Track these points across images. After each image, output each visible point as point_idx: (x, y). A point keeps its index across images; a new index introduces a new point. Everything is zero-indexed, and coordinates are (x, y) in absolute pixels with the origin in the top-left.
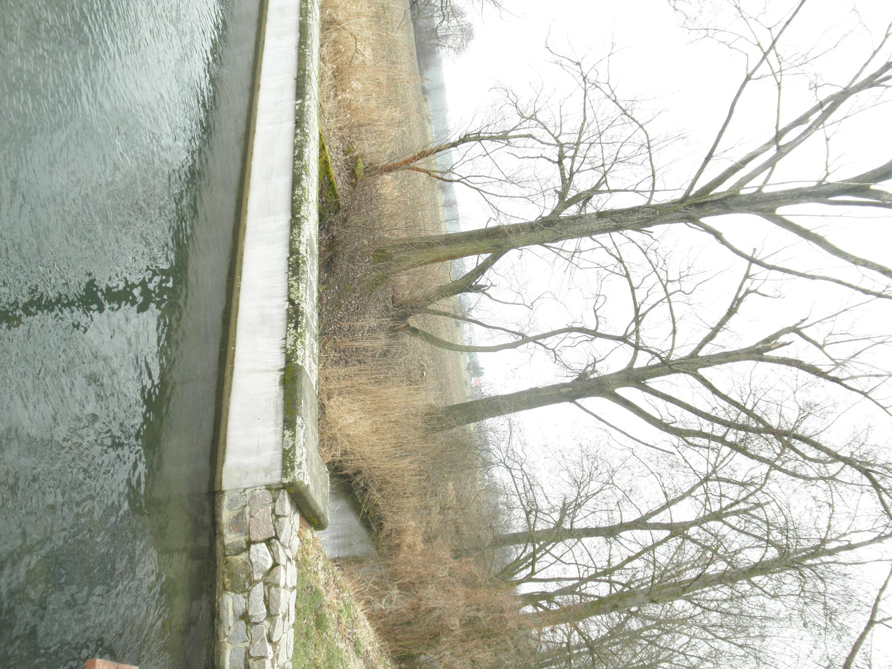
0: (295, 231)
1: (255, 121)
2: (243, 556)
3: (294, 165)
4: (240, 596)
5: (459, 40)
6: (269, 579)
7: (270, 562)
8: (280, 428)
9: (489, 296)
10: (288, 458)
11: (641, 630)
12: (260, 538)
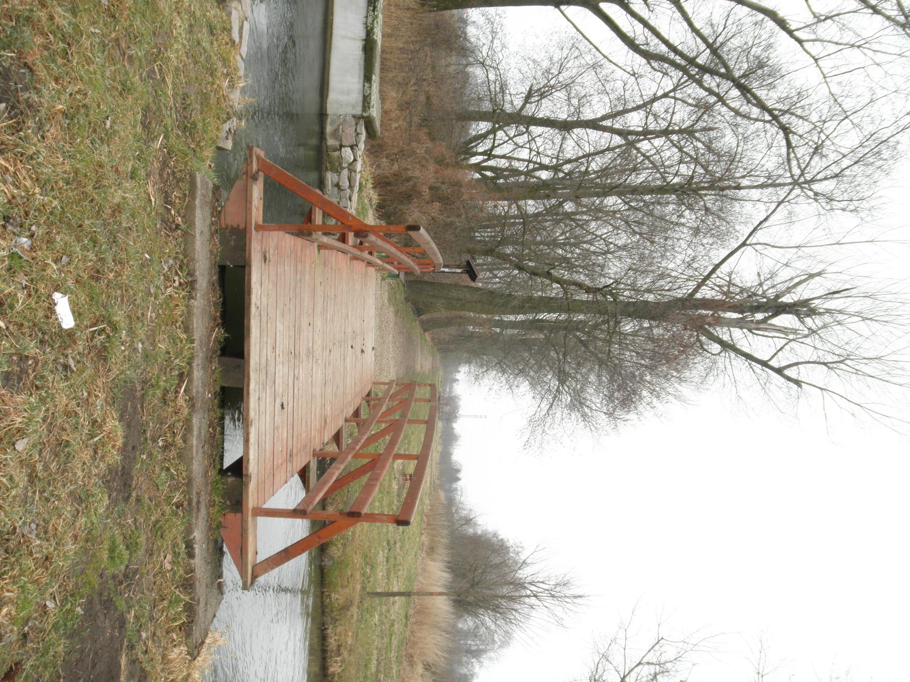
2: (337, 153)
4: (335, 174)
6: (351, 167)
7: (352, 158)
8: (362, 80)
10: (366, 100)
11: (573, 213)
12: (347, 144)
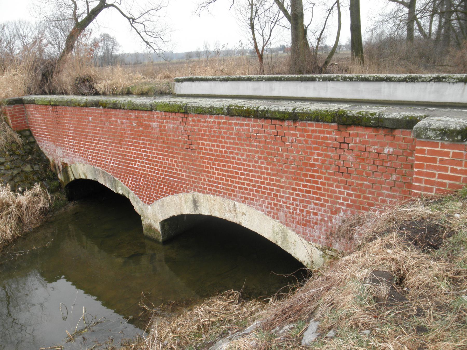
0: (393, 79)
3: (355, 81)
5: (109, 43)
9: (308, 25)
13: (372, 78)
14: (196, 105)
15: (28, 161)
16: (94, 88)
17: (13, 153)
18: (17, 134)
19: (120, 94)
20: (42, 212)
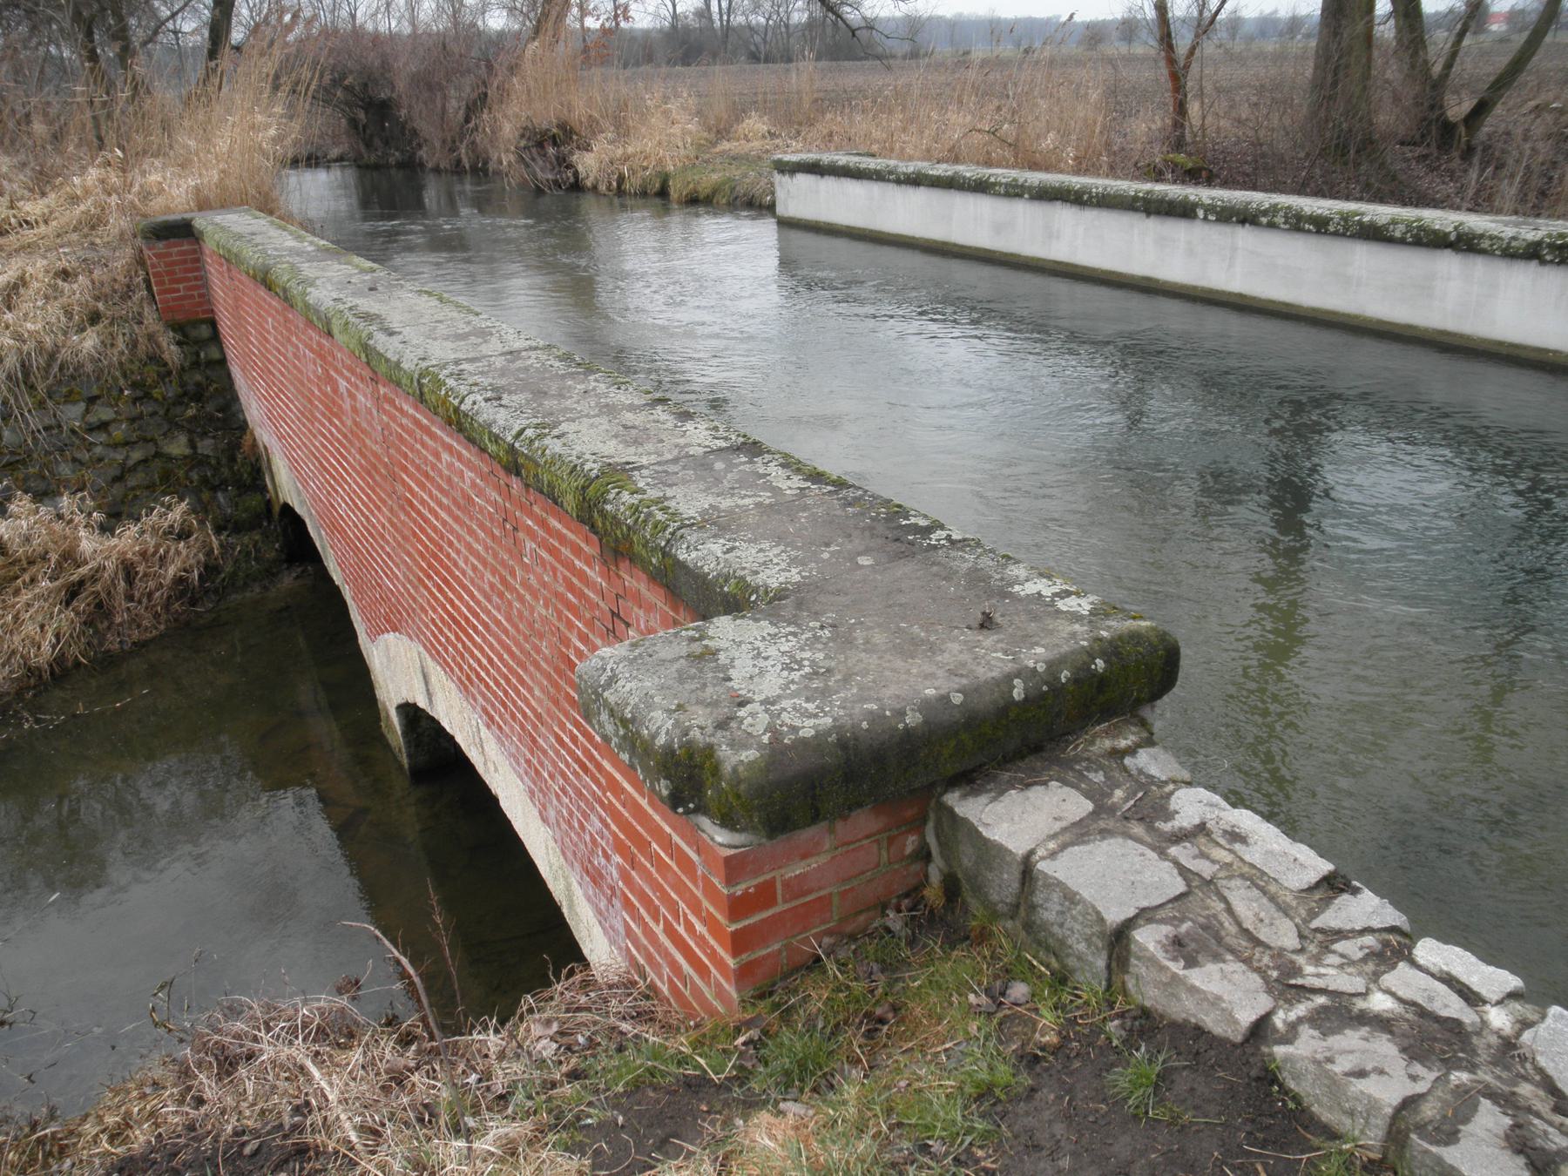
0: (1485, 244)
1: (1217, 291)
3: (1336, 234)
13: (1401, 228)
14: (1171, 196)
15: (185, 423)
16: (569, 166)
17: (143, 393)
18: (171, 334)
19: (644, 194)
20: (182, 594)
